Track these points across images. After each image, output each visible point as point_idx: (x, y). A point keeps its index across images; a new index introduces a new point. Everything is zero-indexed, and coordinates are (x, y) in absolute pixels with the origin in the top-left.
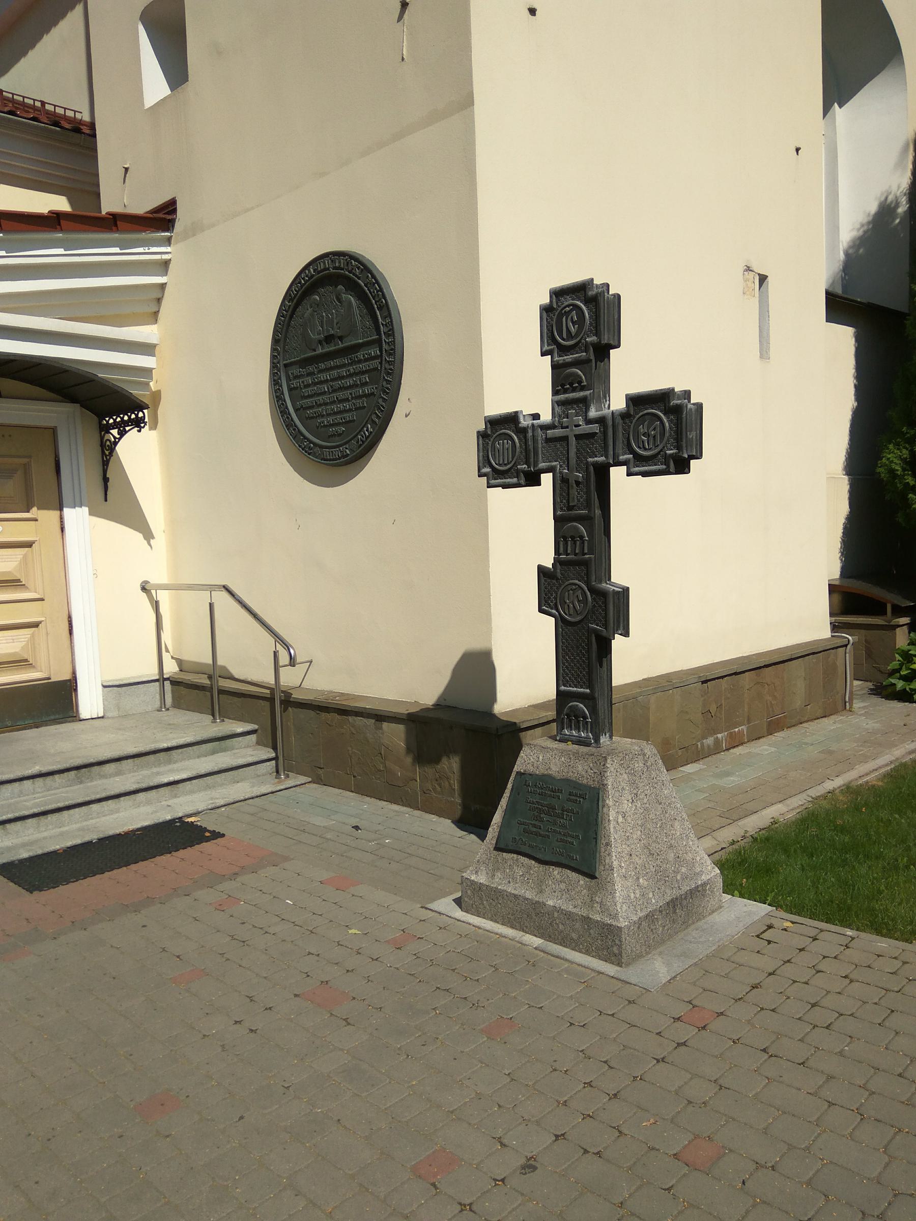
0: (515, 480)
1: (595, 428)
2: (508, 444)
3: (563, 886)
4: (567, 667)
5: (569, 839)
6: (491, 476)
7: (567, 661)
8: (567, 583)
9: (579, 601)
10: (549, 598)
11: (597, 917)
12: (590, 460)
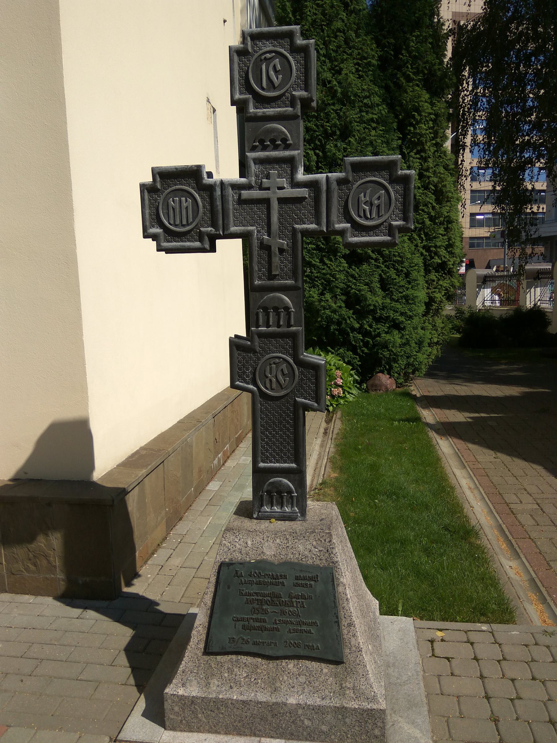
0: (197, 244)
1: (303, 192)
2: (187, 203)
3: (302, 679)
4: (267, 443)
5: (304, 628)
6: (162, 237)
7: (267, 437)
8: (268, 356)
9: (283, 374)
10: (244, 373)
11: (354, 705)
12: (297, 226)
